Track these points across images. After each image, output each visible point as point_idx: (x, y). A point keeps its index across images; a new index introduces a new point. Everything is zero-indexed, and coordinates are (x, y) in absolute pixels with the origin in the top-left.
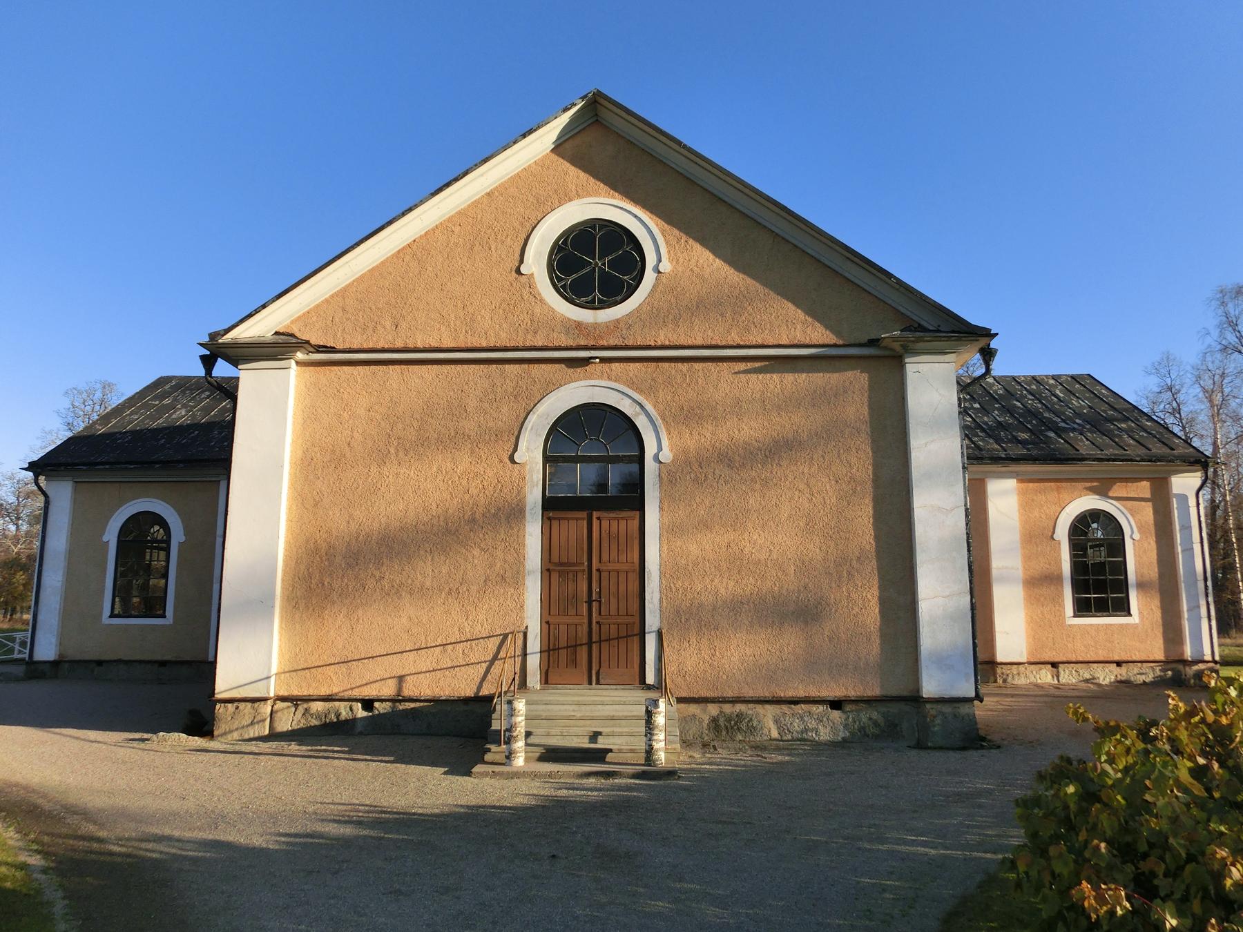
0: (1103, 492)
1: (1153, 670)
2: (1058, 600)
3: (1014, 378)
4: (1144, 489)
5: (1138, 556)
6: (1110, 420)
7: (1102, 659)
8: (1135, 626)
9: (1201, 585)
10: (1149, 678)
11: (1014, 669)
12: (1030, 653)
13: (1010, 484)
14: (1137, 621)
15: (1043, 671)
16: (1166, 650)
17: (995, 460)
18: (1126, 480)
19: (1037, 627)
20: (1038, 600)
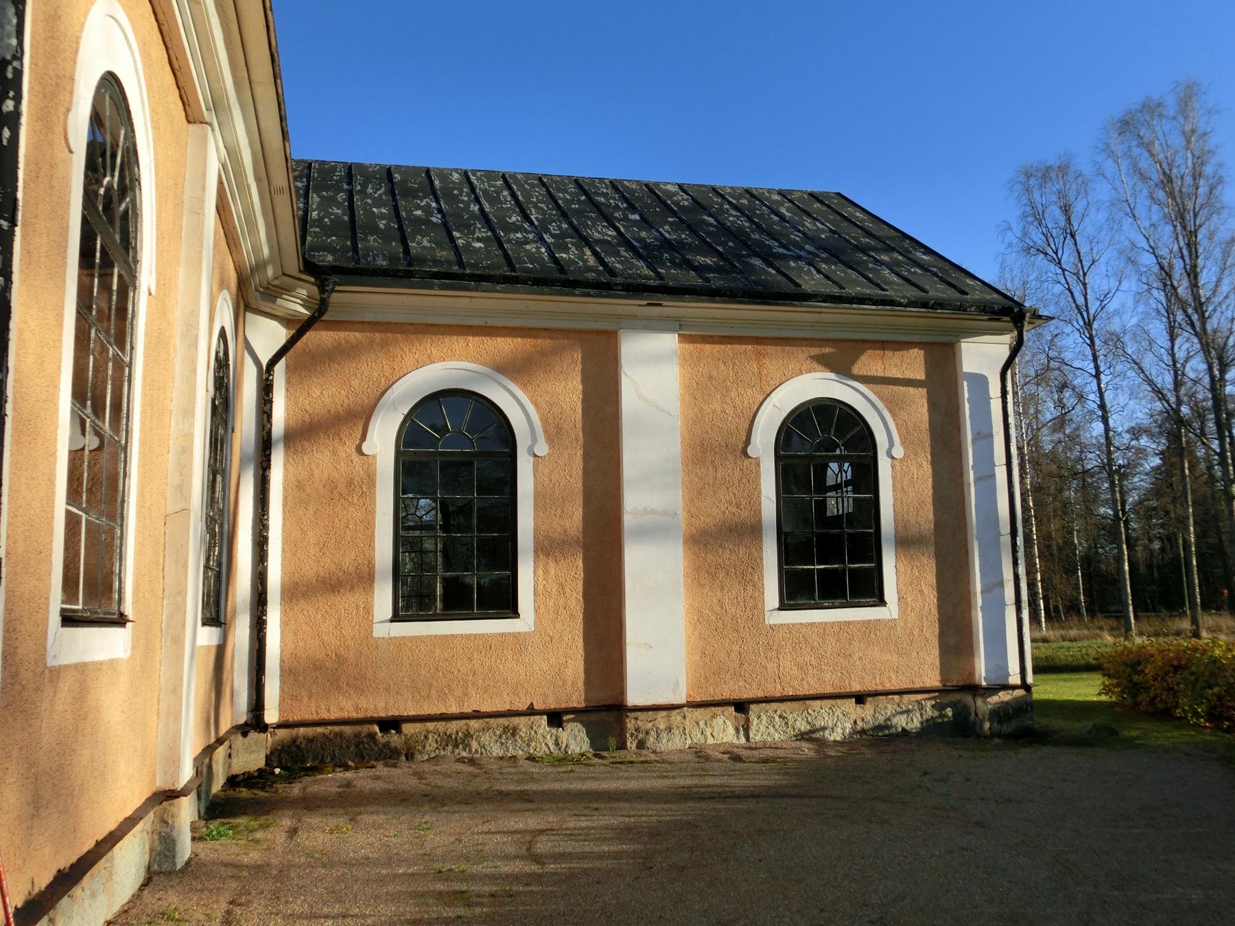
0: (842, 368)
1: (921, 707)
2: (749, 574)
3: (714, 190)
4: (912, 364)
5: (901, 484)
6: (864, 250)
7: (829, 690)
8: (890, 624)
9: (1006, 540)
10: (914, 723)
11: (661, 719)
12: (695, 685)
13: (668, 341)
14: (895, 615)
15: (719, 721)
16: (944, 669)
17: (635, 289)
18: (883, 345)
19: (715, 630)
20: (713, 577)
